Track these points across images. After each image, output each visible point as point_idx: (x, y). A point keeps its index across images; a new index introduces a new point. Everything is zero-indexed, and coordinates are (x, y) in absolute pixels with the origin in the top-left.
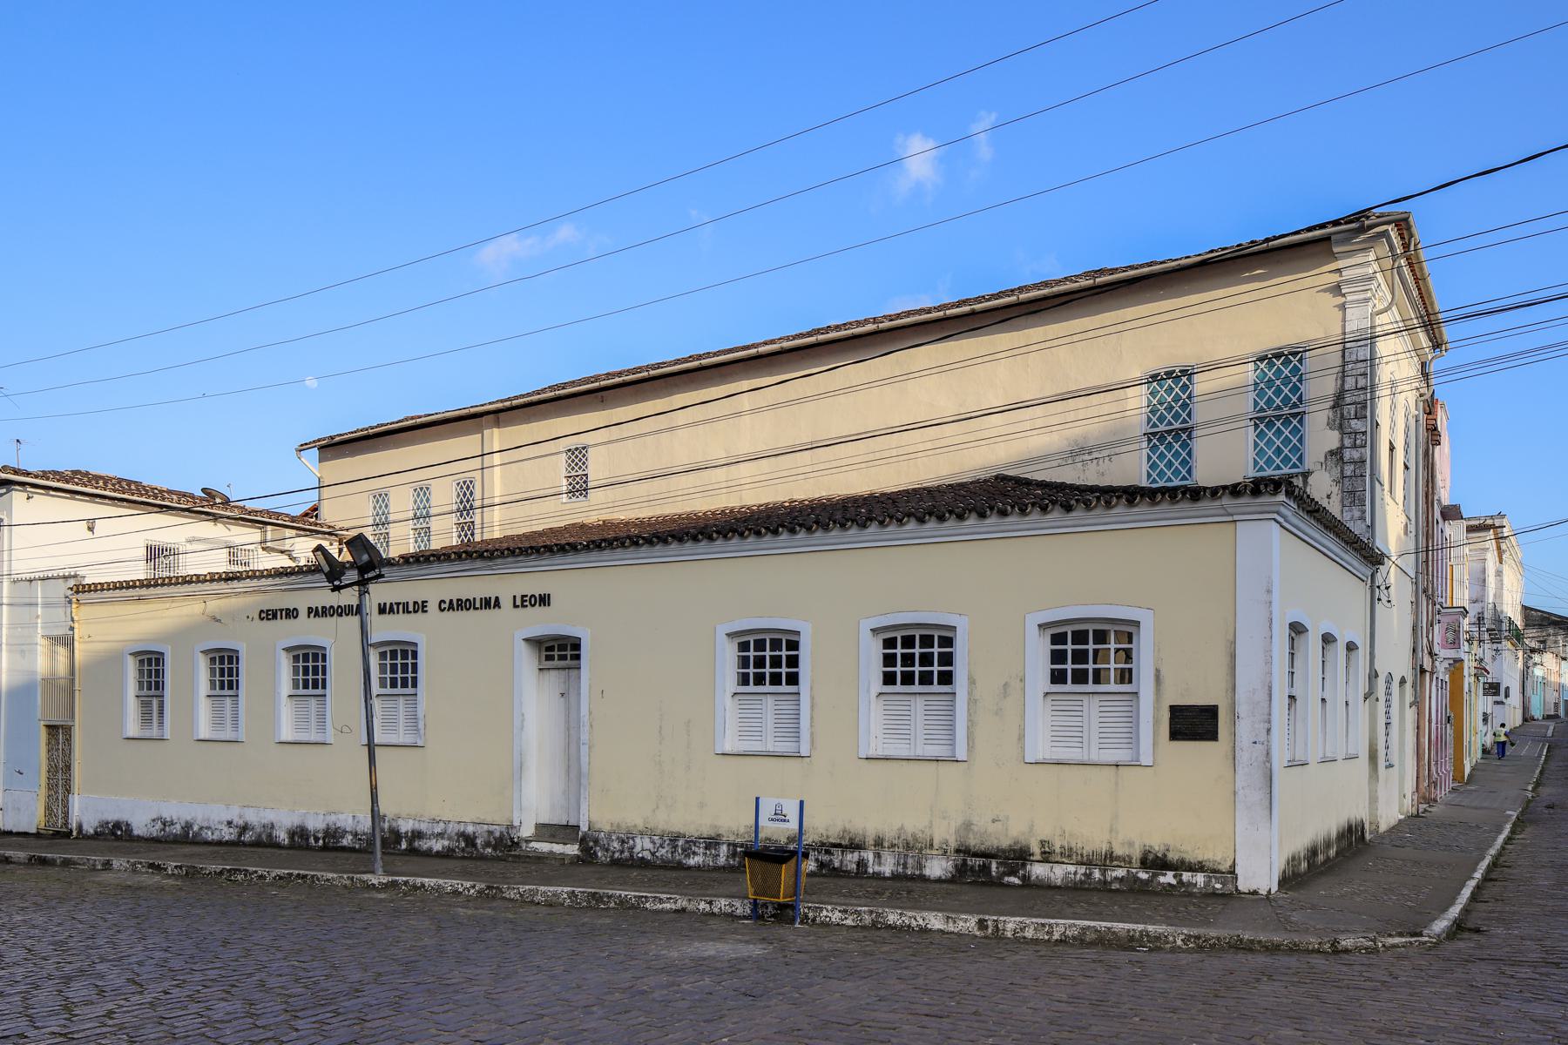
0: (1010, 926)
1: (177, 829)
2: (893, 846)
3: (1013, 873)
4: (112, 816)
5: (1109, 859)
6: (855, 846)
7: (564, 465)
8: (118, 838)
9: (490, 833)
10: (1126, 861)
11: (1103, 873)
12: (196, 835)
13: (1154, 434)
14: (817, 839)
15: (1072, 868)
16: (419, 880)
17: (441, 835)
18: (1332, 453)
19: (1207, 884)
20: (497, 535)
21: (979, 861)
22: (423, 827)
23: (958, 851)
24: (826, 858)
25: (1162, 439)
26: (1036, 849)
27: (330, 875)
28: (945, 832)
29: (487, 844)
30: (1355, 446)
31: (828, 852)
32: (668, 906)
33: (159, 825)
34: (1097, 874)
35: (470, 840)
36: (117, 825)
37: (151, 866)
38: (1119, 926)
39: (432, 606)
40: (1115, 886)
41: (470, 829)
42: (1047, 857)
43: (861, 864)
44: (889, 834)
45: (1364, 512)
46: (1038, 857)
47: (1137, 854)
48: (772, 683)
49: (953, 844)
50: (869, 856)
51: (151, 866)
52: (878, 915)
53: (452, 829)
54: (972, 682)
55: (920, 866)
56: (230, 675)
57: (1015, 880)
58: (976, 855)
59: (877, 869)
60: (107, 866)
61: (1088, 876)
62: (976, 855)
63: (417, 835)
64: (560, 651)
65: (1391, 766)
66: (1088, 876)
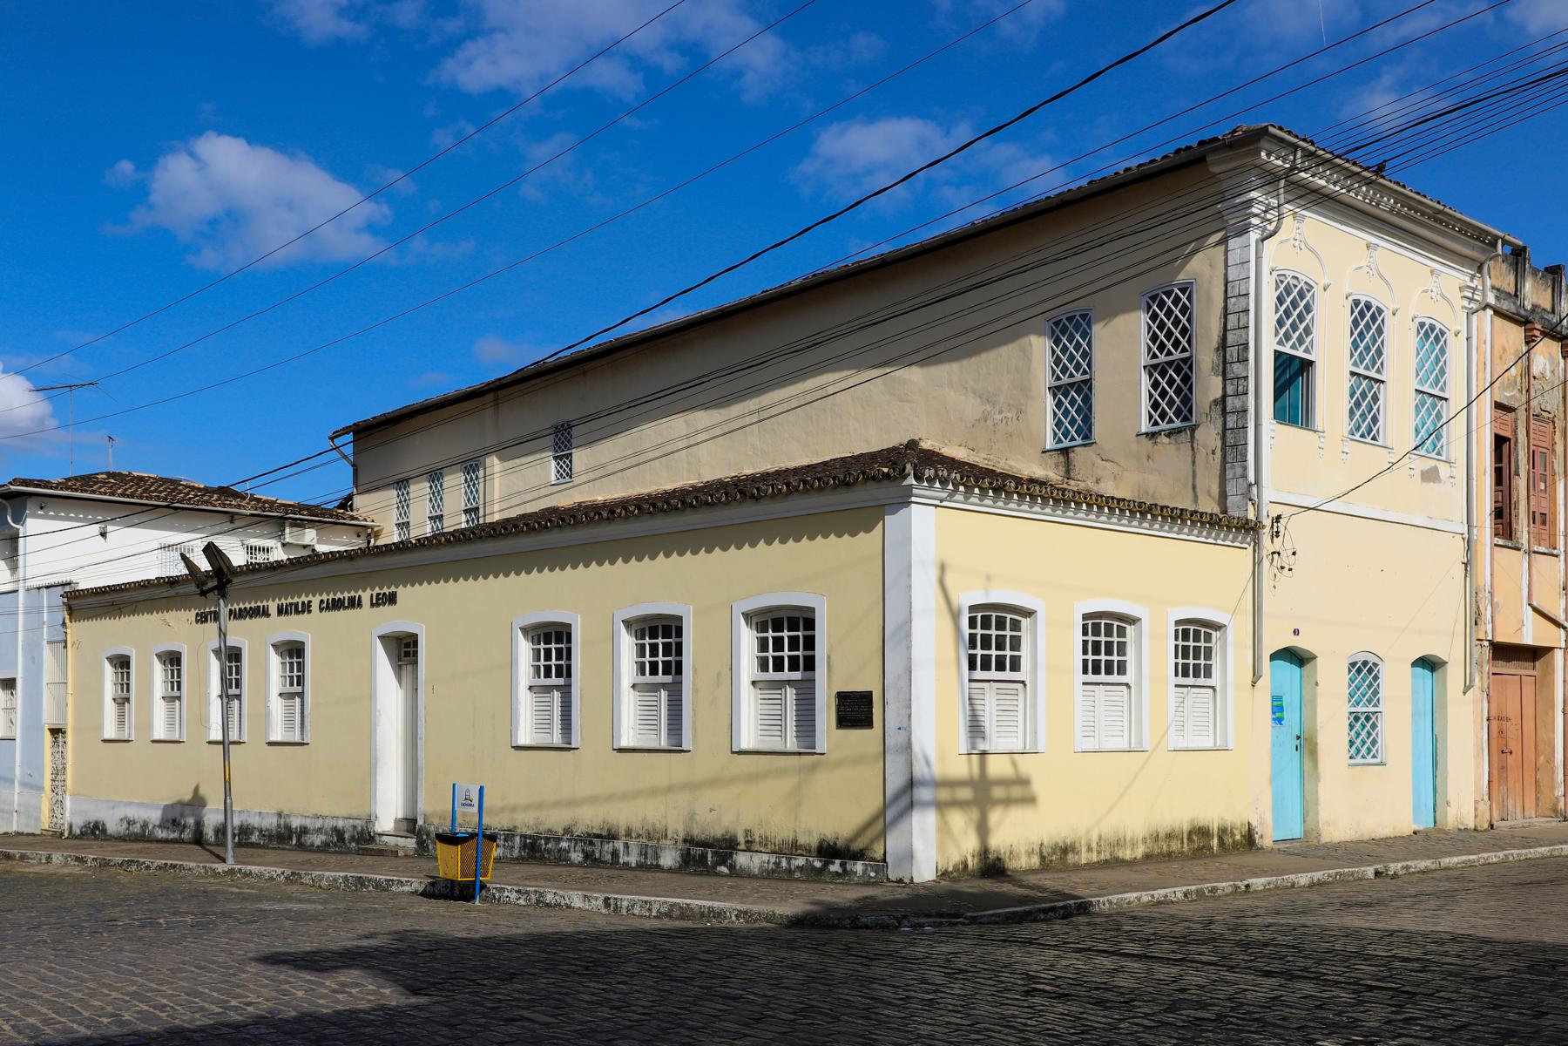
0: (625, 904)
1: (137, 829)
2: (639, 836)
3: (723, 863)
4: (93, 817)
5: (793, 848)
6: (611, 836)
7: (1144, 338)
8: (96, 838)
9: (354, 827)
10: (807, 851)
11: (789, 860)
12: (151, 833)
13: (1155, 367)
14: (585, 830)
15: (765, 857)
16: (249, 868)
17: (319, 830)
18: (1215, 402)
19: (865, 872)
20: (497, 517)
21: (699, 850)
22: (308, 823)
23: (685, 841)
24: (589, 848)
25: (1163, 373)
26: (741, 839)
27: (192, 865)
28: (676, 826)
29: (352, 839)
30: (1237, 395)
31: (591, 843)
32: (406, 888)
33: (125, 825)
34: (784, 863)
35: (339, 833)
36: (96, 825)
37: (77, 859)
38: (695, 903)
39: (315, 606)
40: (797, 875)
41: (340, 824)
42: (749, 847)
43: (615, 854)
44: (636, 826)
45: (1245, 469)
46: (742, 847)
47: (814, 842)
48: (775, 670)
49: (682, 835)
50: (619, 845)
51: (77, 859)
52: (541, 894)
53: (329, 823)
54: (695, 671)
55: (657, 856)
56: (1186, 649)
57: (724, 869)
58: (698, 844)
59: (626, 859)
60: (49, 858)
61: (777, 864)
62: (698, 844)
63: (304, 831)
64: (404, 649)
65: (56, 732)
66: (777, 864)
